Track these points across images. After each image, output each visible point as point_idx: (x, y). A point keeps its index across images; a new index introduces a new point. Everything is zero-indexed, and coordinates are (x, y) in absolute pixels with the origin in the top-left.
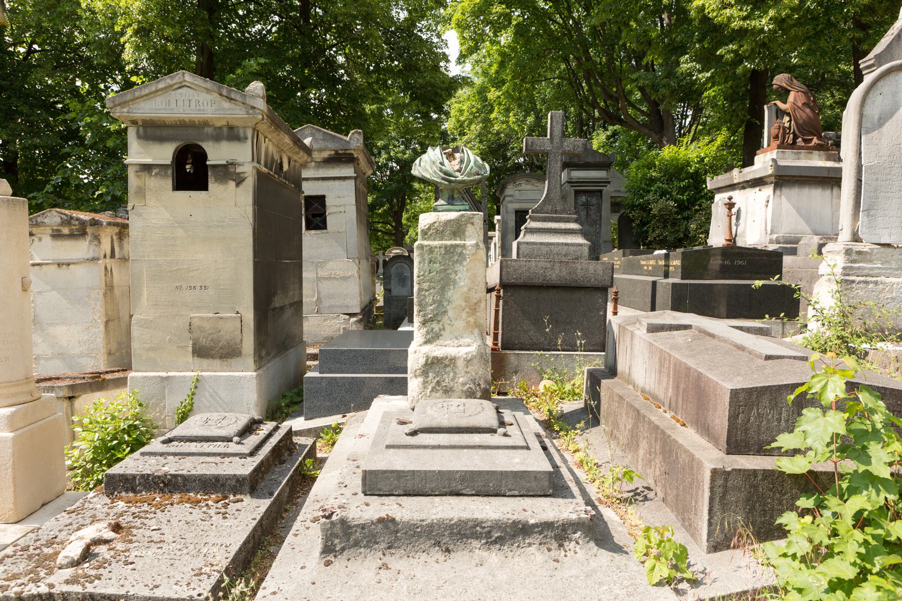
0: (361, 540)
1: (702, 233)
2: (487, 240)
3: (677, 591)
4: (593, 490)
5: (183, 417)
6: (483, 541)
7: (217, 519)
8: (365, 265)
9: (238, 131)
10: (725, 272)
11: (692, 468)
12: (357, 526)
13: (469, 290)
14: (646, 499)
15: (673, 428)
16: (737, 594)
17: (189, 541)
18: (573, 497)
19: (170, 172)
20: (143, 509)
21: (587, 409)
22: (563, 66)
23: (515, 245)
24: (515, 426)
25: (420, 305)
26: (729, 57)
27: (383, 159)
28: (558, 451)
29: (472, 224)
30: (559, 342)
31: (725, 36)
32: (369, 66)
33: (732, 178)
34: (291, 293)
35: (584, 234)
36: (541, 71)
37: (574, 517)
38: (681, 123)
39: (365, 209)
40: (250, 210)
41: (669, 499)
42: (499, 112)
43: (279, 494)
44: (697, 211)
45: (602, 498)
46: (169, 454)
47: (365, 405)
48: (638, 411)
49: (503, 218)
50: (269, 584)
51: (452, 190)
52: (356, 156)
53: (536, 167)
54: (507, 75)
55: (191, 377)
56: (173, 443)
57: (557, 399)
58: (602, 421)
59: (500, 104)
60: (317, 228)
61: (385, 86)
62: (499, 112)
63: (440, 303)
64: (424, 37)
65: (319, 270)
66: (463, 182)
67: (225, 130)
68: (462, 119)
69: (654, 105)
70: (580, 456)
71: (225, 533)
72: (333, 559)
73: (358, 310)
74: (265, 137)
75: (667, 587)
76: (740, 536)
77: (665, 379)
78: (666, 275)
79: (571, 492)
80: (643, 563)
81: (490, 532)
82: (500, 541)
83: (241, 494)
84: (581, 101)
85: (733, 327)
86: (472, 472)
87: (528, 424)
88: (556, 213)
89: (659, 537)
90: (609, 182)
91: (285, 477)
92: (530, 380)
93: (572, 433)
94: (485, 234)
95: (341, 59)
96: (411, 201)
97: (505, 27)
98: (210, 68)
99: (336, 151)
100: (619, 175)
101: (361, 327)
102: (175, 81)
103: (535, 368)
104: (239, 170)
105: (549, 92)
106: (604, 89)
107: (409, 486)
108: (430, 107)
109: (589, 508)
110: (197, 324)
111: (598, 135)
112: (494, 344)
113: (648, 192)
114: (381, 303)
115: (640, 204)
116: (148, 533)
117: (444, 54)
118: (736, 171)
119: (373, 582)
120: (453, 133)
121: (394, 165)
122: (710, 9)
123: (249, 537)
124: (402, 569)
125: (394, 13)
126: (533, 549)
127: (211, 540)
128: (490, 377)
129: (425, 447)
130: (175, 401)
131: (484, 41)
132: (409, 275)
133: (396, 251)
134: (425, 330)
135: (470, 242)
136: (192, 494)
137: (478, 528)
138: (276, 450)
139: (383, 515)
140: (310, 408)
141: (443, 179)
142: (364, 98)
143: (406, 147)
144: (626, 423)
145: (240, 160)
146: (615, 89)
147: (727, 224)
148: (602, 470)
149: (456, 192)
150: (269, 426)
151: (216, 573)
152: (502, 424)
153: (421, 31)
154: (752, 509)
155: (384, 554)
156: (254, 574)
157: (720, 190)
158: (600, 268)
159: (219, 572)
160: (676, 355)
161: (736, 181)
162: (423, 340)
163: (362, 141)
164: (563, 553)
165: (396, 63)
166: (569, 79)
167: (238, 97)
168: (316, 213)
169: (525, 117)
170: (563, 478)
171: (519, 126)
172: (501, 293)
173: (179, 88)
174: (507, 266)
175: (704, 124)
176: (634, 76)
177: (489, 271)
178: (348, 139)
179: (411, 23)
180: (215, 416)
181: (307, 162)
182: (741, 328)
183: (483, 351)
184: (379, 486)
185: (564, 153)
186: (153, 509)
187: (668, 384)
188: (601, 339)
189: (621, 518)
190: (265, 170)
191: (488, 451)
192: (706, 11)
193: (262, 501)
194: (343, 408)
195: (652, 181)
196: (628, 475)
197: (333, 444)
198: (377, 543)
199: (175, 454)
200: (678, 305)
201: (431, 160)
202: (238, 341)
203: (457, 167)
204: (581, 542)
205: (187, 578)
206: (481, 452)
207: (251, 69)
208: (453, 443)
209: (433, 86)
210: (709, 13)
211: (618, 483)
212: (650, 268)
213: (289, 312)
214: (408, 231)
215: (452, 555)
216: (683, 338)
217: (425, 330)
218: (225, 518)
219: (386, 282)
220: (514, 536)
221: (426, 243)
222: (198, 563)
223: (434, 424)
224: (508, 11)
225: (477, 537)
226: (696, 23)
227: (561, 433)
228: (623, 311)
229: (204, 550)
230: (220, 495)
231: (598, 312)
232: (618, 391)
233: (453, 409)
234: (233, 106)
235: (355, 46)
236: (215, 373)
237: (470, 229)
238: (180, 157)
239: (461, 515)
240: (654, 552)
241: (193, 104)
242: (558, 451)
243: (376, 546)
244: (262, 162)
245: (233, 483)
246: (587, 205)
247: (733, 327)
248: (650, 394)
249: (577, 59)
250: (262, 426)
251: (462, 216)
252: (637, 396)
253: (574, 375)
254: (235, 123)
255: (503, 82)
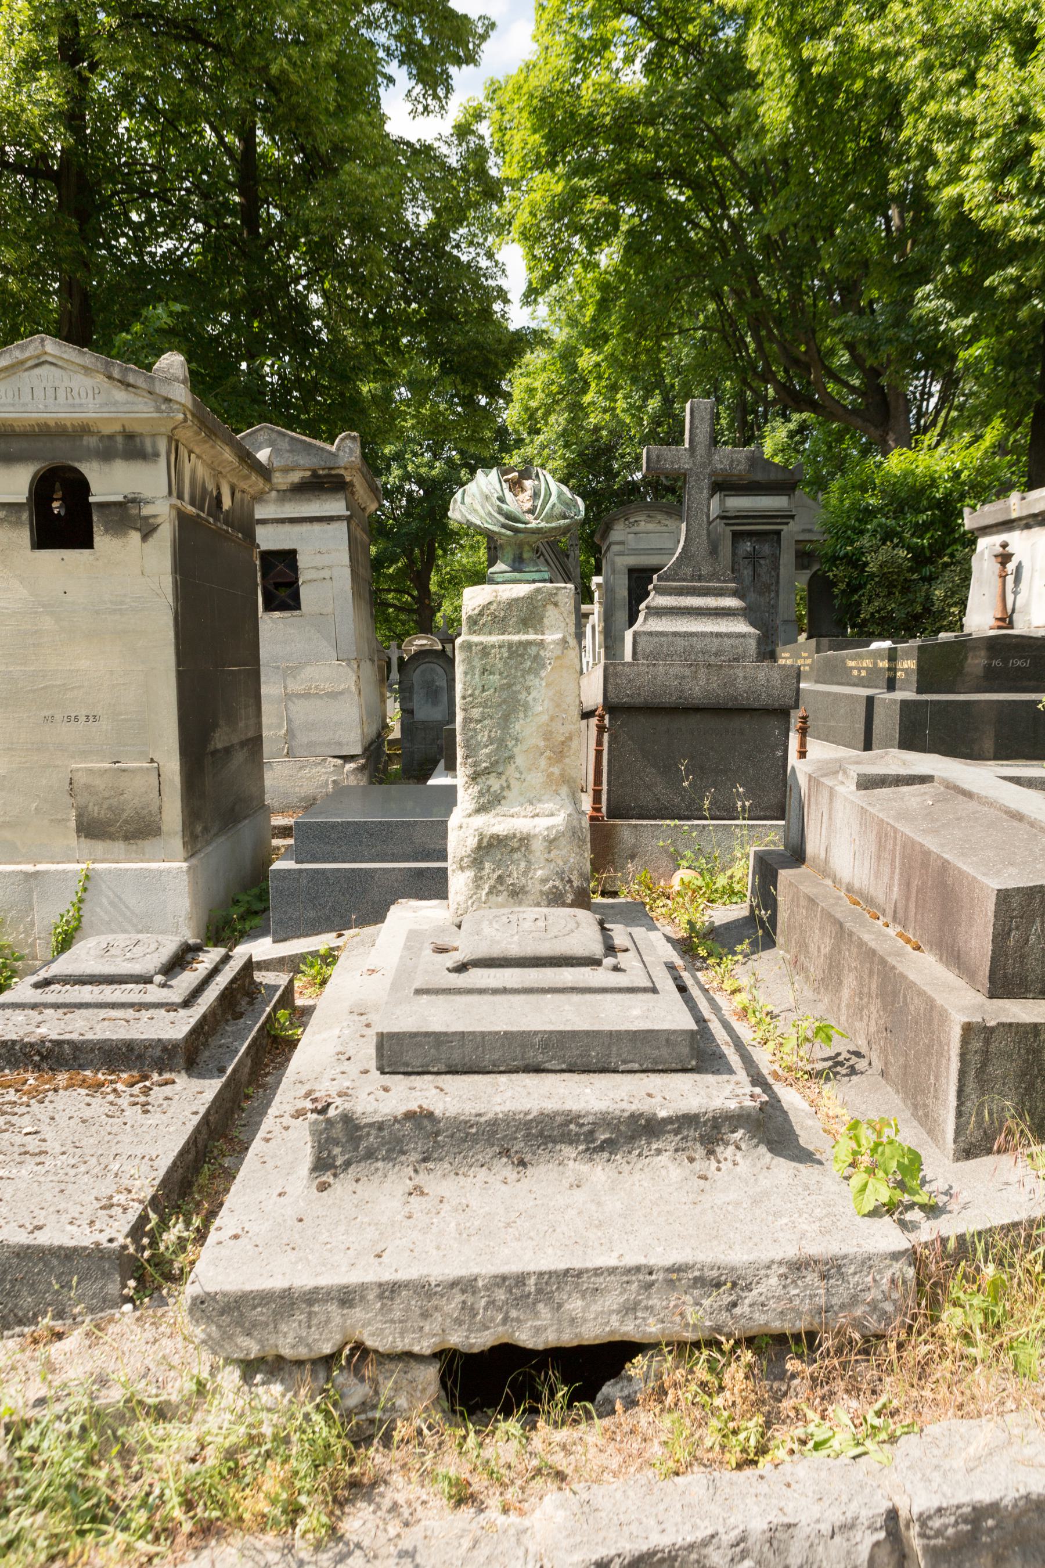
0: (378, 1149)
1: (955, 604)
2: (581, 618)
3: (903, 1224)
4: (763, 1058)
5: (65, 943)
6: (581, 1147)
7: (133, 1114)
8: (369, 671)
9: (142, 443)
10: (992, 680)
11: (930, 1022)
12: (371, 1125)
13: (552, 719)
14: (853, 1071)
15: (899, 954)
16: (1002, 1228)
17: (88, 1151)
18: (731, 1071)
19: (25, 516)
20: (7, 1098)
21: (751, 920)
22: (712, 307)
23: (629, 635)
24: (632, 954)
25: (467, 746)
26: (1006, 289)
27: (393, 477)
28: (705, 991)
29: (556, 604)
30: (707, 804)
31: (997, 250)
32: (366, 314)
33: (1008, 509)
34: (242, 724)
35: (748, 614)
36: (673, 316)
37: (732, 1105)
38: (920, 407)
39: (365, 572)
40: (167, 582)
41: (892, 1071)
42: (599, 392)
43: (234, 1071)
44: (946, 565)
45: (780, 1072)
46: (46, 1006)
47: (376, 915)
48: (841, 925)
49: (606, 581)
50: (226, 1222)
51: (520, 546)
52: (348, 479)
53: (666, 492)
54: (613, 325)
55: (76, 872)
56: (53, 987)
57: (702, 901)
58: (780, 939)
59: (600, 377)
60: (283, 607)
61: (395, 348)
62: (599, 392)
63: (501, 743)
64: (464, 258)
65: (289, 680)
66: (538, 531)
67: (119, 439)
68: (533, 404)
69: (873, 374)
70: (741, 999)
71: (148, 1138)
72: (331, 1180)
73: (358, 750)
74: (190, 452)
75: (887, 1218)
76: (1010, 1132)
77: (886, 870)
78: (891, 685)
79: (728, 1063)
80: (847, 1178)
81: (591, 1132)
82: (610, 1146)
83: (171, 1070)
84: (744, 370)
85: (1005, 778)
86: (560, 1032)
87: (654, 946)
88: (700, 580)
89: (874, 1137)
90: (792, 517)
91: (243, 1043)
92: (656, 869)
93: (728, 961)
94: (577, 609)
95: (316, 300)
96: (445, 551)
97: (607, 237)
98: (85, 325)
99: (314, 472)
100: (810, 502)
101: (363, 780)
102: (27, 354)
103: (665, 849)
104: (146, 511)
105: (686, 355)
106: (782, 346)
107: (456, 1057)
108: (475, 386)
109: (758, 1090)
110: (83, 781)
111: (773, 430)
112: (595, 809)
113: (862, 532)
114: (396, 734)
115: (846, 555)
116: (19, 1139)
117: (500, 289)
118: (1015, 496)
119: (399, 1218)
120: (517, 432)
121: (415, 487)
122: (972, 204)
123: (187, 1143)
124: (447, 1194)
125: (409, 216)
126: (664, 1159)
127: (126, 1150)
128: (588, 866)
129: (481, 991)
130: (50, 913)
131: (570, 263)
132: (444, 684)
133: (421, 642)
134: (477, 788)
135: (552, 637)
136: (88, 1073)
137: (572, 1126)
138: (227, 997)
139: (414, 1106)
140: (280, 922)
141: (504, 526)
142: (360, 370)
143: (435, 455)
144: (821, 944)
145: (147, 493)
146: (803, 348)
147: (999, 590)
148: (780, 1022)
149: (526, 548)
150: (212, 956)
151: (136, 1204)
152: (611, 949)
153: (458, 246)
154: (1031, 1088)
155: (416, 1171)
156: (198, 1204)
157: (986, 530)
158: (776, 676)
159: (141, 1202)
160: (906, 829)
161: (1014, 515)
162: (473, 806)
163: (358, 452)
164: (714, 1165)
165: (414, 306)
166: (722, 331)
167: (140, 382)
168: (282, 582)
169: (645, 399)
170: (714, 1040)
171: (633, 416)
172: (607, 722)
173: (37, 366)
174: (616, 675)
175: (961, 408)
176: (834, 324)
177: (584, 681)
178: (334, 449)
179: (440, 231)
180: (121, 939)
181: (263, 492)
182: (1017, 781)
183: (575, 823)
184: (406, 1058)
185: (714, 473)
186: (25, 1099)
187: (892, 878)
188: (777, 798)
189: (812, 1103)
190: (191, 509)
191: (588, 997)
192: (966, 207)
193: (207, 1082)
194: (338, 922)
195: (869, 513)
196: (823, 1032)
197: (324, 982)
198: (404, 1153)
199: (56, 1006)
200: (912, 738)
201: (482, 492)
202: (154, 809)
203: (528, 505)
204: (743, 1146)
205: (88, 1212)
206: (576, 998)
207: (158, 324)
208: (527, 985)
209: (480, 347)
210: (971, 210)
211: (807, 1046)
212: (863, 673)
213: (239, 757)
214: (440, 605)
215: (530, 1171)
216: (919, 799)
217: (477, 788)
218: (147, 1112)
219: (405, 695)
220: (632, 1138)
221: (475, 639)
222: (106, 1188)
223: (496, 952)
224: (613, 207)
225: (571, 1140)
226: (946, 227)
227: (711, 961)
228: (817, 749)
229: (115, 1167)
230: (135, 1073)
231: (773, 751)
232: (807, 889)
233: (527, 925)
234: (131, 397)
235: (343, 278)
236: (115, 864)
237: (551, 615)
238: (42, 489)
239: (544, 1105)
240: (865, 1160)
241: (61, 394)
242: (705, 991)
243: (403, 1158)
244: (187, 497)
245: (158, 1052)
246: (753, 558)
247: (1005, 778)
248: (860, 894)
249: (738, 293)
250: (202, 956)
251: (538, 591)
252: (839, 898)
253: (733, 860)
254: (138, 429)
255: (606, 337)
